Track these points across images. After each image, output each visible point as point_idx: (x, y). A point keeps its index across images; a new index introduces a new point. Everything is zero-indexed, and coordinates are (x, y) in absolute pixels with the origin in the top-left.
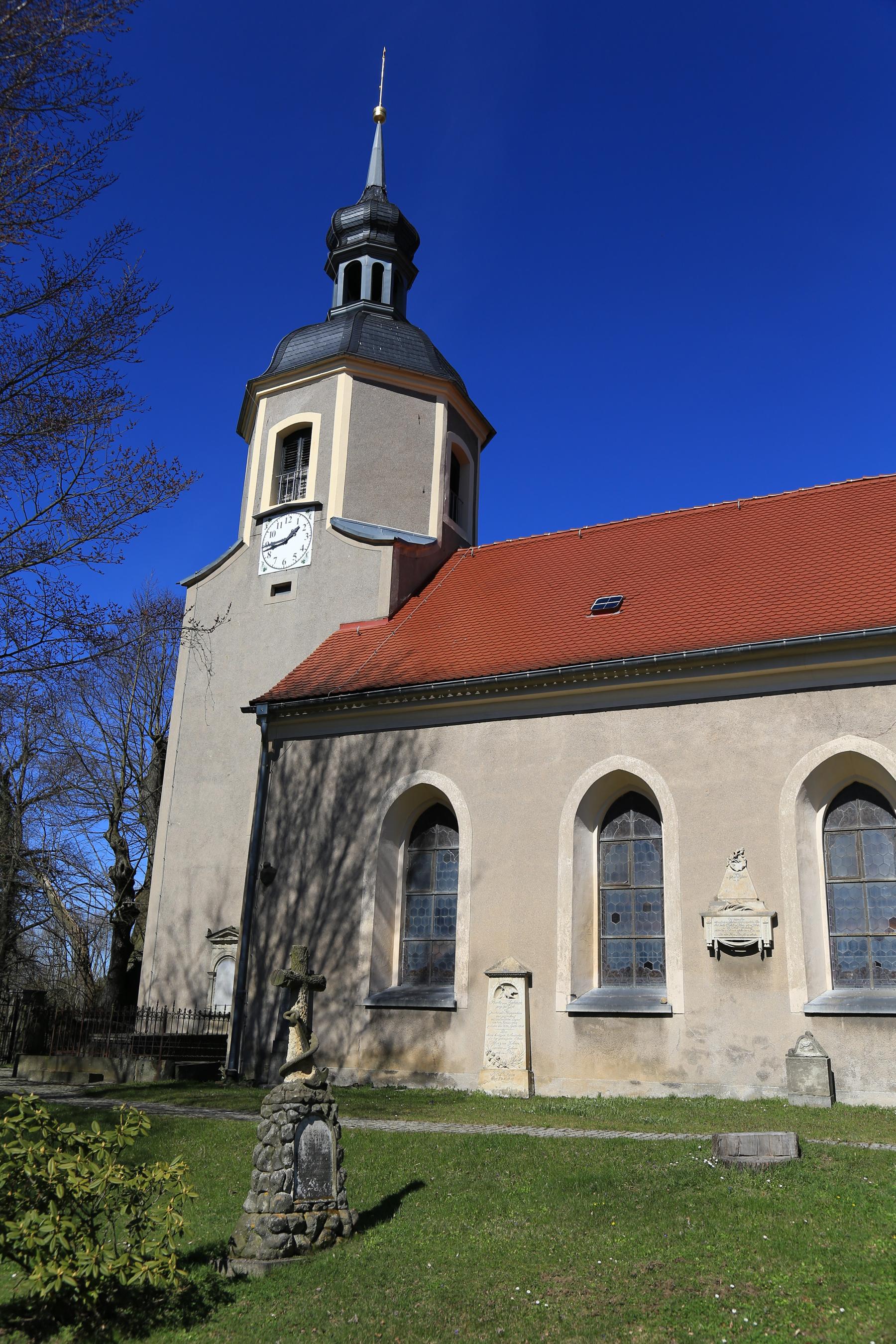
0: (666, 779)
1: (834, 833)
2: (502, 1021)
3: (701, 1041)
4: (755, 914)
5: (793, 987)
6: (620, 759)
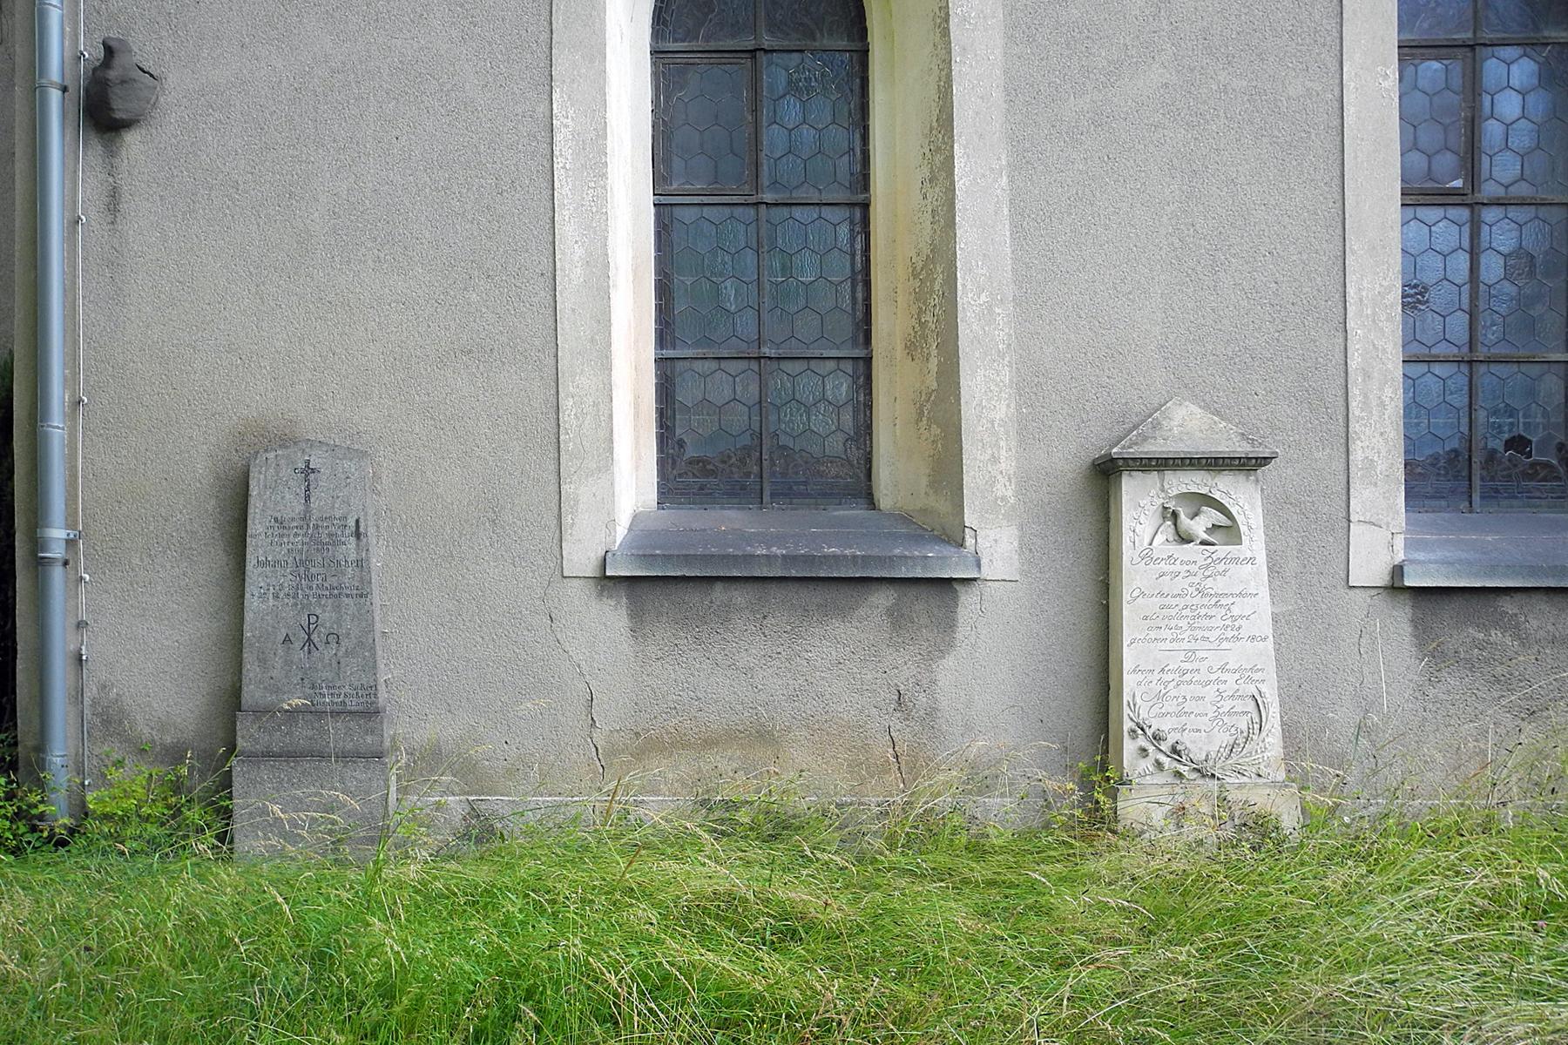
2: (1183, 623)
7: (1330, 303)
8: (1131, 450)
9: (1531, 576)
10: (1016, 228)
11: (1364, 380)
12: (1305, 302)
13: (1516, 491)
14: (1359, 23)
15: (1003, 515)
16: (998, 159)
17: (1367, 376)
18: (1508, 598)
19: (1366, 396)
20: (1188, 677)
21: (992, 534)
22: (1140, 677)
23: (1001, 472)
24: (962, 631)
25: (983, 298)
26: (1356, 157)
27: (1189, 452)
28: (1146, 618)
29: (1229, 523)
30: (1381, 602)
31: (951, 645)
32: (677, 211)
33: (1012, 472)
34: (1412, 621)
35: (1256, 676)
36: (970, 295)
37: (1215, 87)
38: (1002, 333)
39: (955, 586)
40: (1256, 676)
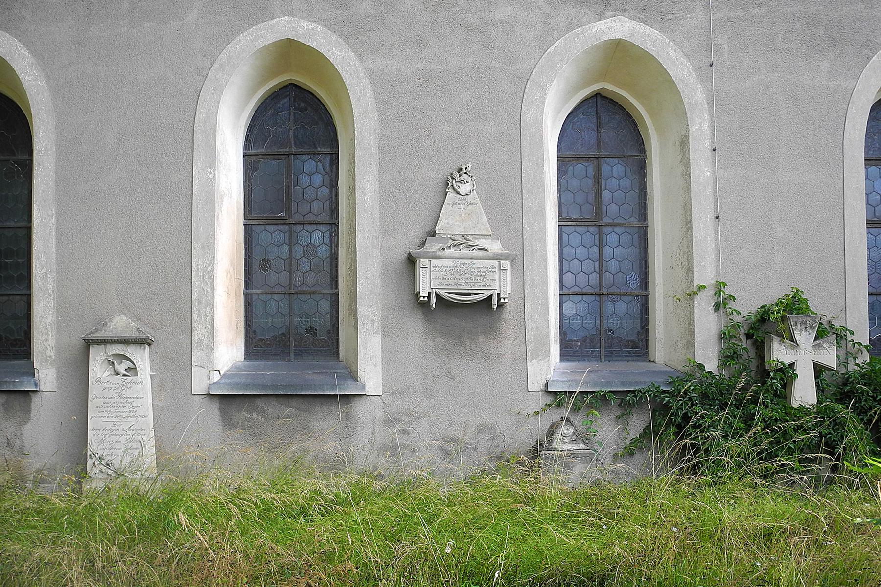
0: (361, 57)
1: (567, 160)
2: (113, 410)
3: (405, 432)
4: (491, 255)
5: (532, 359)
6: (290, 22)
7: (186, 271)
8: (89, 336)
9: (264, 390)
10: (58, 240)
11: (198, 304)
12: (176, 271)
13: (620, 353)
14: (200, 150)
15: (50, 363)
16: (52, 211)
17: (200, 302)
18: (259, 399)
19: (199, 311)
20: (114, 433)
21: (45, 372)
22: (94, 432)
23: (49, 345)
24: (33, 414)
25: (43, 271)
26: (197, 207)
27: (113, 337)
28: (97, 407)
29: (134, 367)
30: (206, 401)
31: (29, 419)
32: (254, 228)
33: (54, 345)
34: (220, 409)
35: (141, 433)
36: (38, 269)
37: (141, 178)
38: (51, 286)
39: (30, 394)
40: (141, 433)
